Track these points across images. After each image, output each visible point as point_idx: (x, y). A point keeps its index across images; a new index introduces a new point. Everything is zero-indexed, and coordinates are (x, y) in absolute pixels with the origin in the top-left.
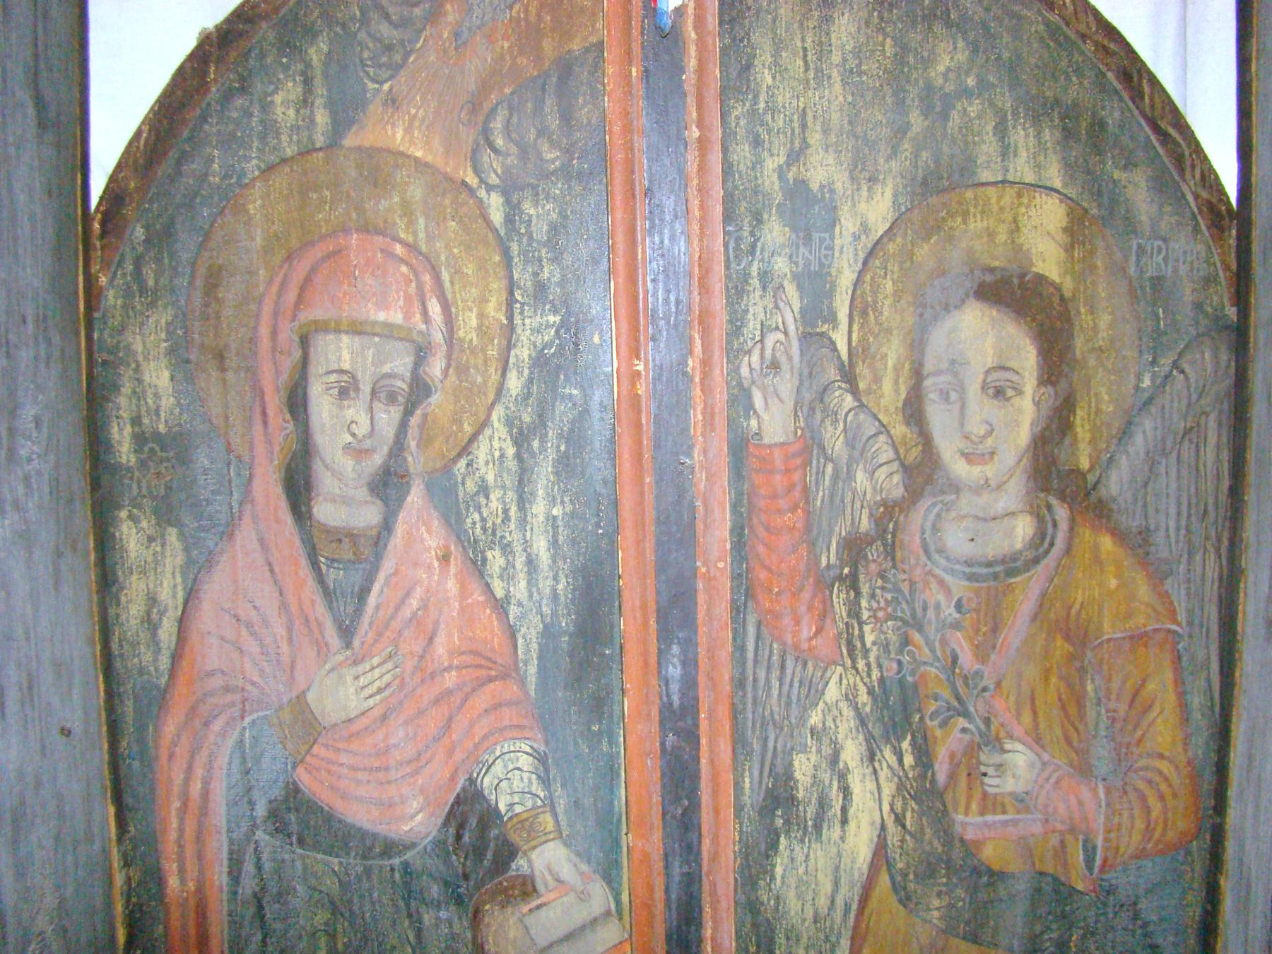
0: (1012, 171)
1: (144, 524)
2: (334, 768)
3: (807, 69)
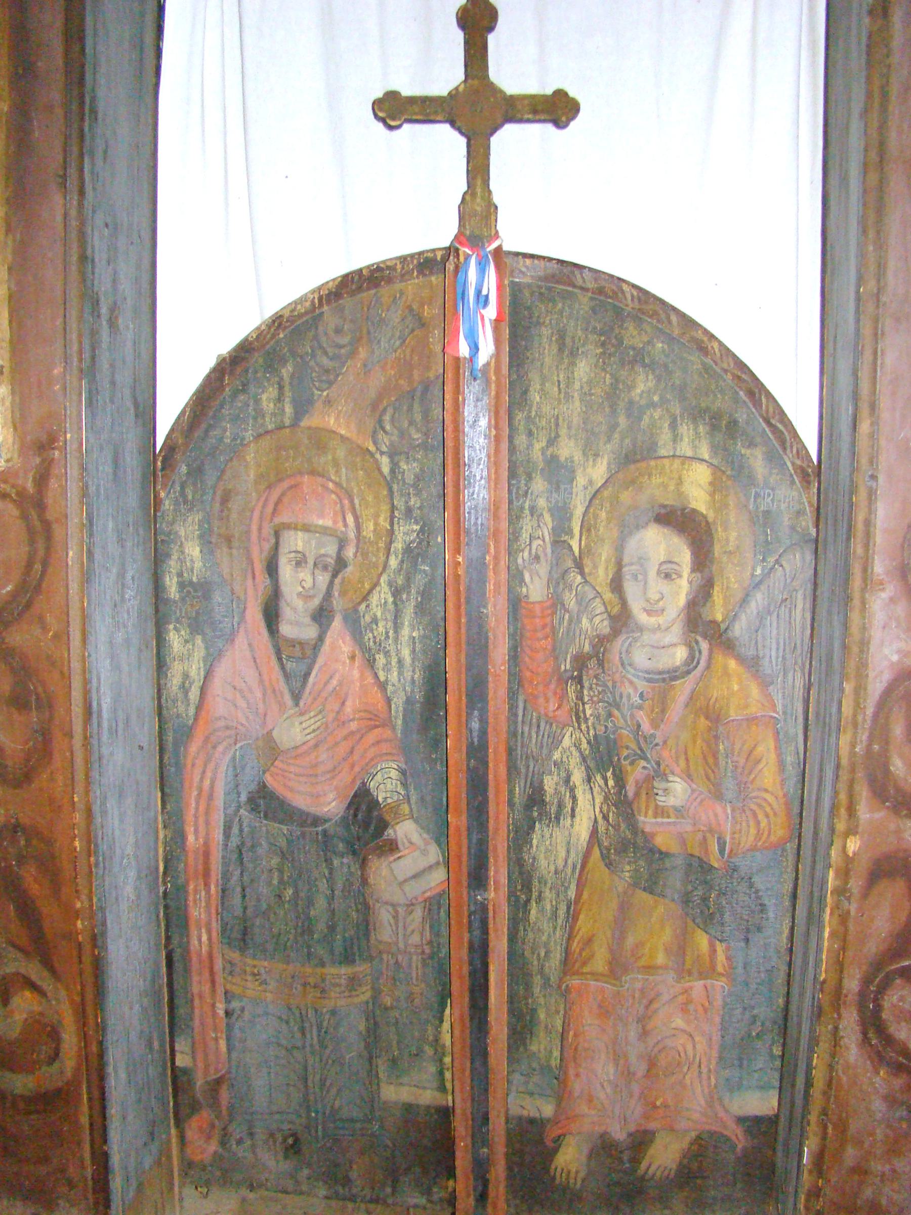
0: (678, 449)
1: (183, 633)
2: (287, 774)
3: (560, 392)
